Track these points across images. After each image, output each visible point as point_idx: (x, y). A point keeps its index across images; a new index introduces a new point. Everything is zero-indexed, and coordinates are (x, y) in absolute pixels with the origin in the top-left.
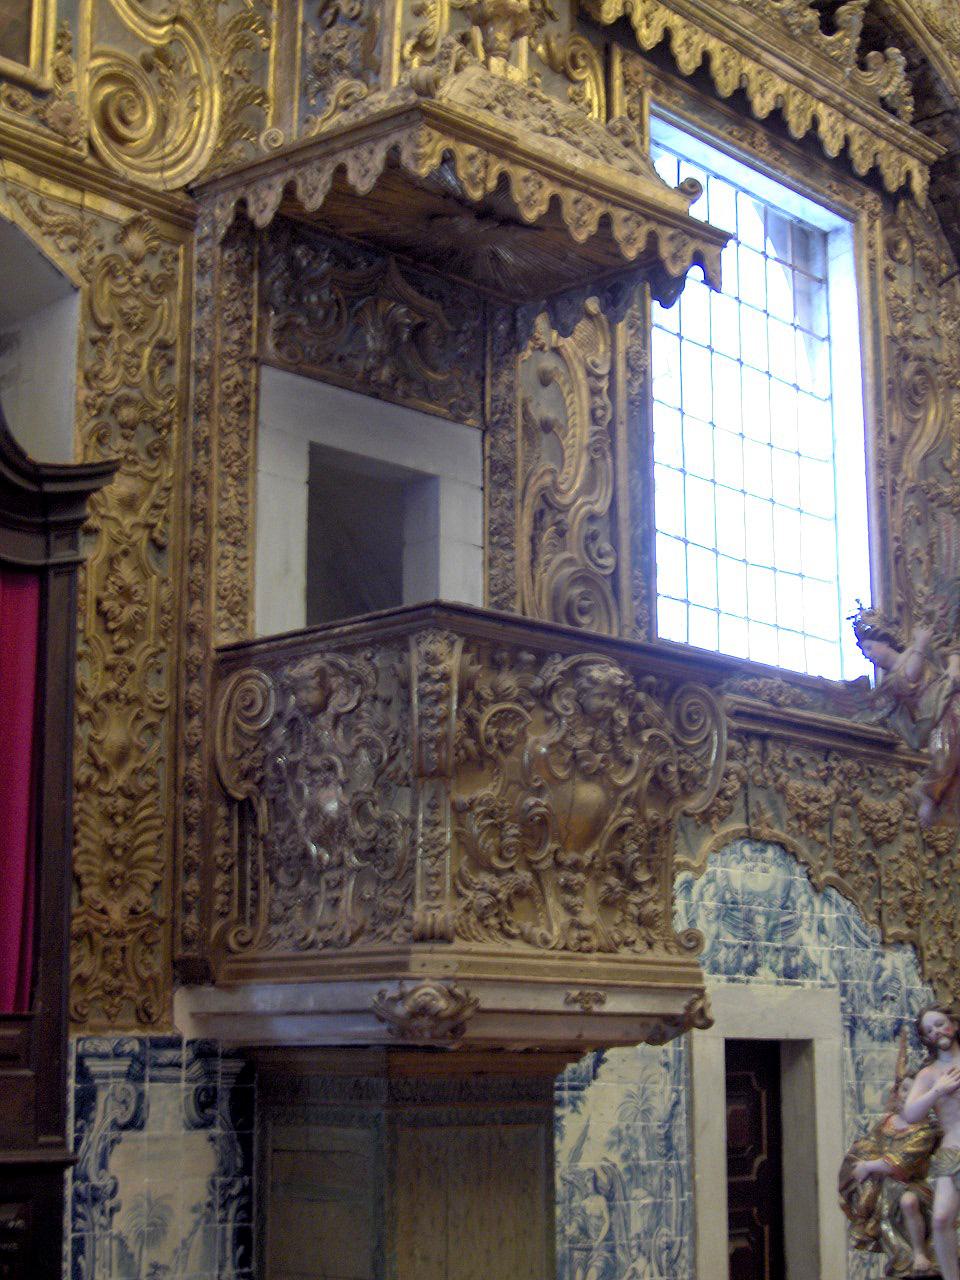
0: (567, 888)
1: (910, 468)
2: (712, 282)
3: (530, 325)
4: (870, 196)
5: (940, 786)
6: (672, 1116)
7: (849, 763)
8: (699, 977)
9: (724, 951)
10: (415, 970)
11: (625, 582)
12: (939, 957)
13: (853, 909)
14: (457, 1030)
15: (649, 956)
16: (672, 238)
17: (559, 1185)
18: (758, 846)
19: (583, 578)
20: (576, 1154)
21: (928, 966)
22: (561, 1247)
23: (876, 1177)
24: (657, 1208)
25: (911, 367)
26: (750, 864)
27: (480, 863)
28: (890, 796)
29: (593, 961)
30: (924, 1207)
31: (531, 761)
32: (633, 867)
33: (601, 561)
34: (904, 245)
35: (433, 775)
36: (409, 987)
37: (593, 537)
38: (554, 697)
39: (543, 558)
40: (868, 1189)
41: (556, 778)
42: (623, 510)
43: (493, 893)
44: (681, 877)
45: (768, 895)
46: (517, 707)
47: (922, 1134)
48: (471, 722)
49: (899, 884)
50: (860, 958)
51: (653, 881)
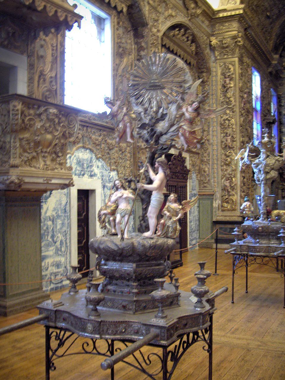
0: (44, 157)
1: (120, 71)
2: (79, 26)
3: (39, 34)
4: (114, 12)
5: (121, 135)
6: (66, 205)
7: (105, 133)
8: (72, 176)
9: (77, 171)
10: (10, 173)
11: (58, 92)
12: (122, 173)
13: (104, 163)
14: (20, 186)
15: (61, 171)
16: (70, 17)
17: (42, 219)
18: (85, 149)
19: (49, 90)
20: (46, 213)
21: (120, 175)
22: (42, 232)
23: (105, 214)
24: (63, 224)
25: (121, 49)
26: (83, 153)
27: (25, 151)
28: (113, 140)
29: (49, 172)
30: (114, 220)
31: (36, 129)
32: (58, 153)
33: (53, 87)
34: (121, 23)
35: (15, 132)
36: (9, 177)
37: (51, 82)
38: (42, 116)
39: (40, 86)
40: (103, 217)
41: (41, 133)
42: (58, 76)
43: (28, 157)
44: (68, 156)
45: (87, 160)
46: (33, 118)
47: (114, 206)
48: (23, 121)
49: (114, 158)
50: (106, 173)
51: (62, 156)
